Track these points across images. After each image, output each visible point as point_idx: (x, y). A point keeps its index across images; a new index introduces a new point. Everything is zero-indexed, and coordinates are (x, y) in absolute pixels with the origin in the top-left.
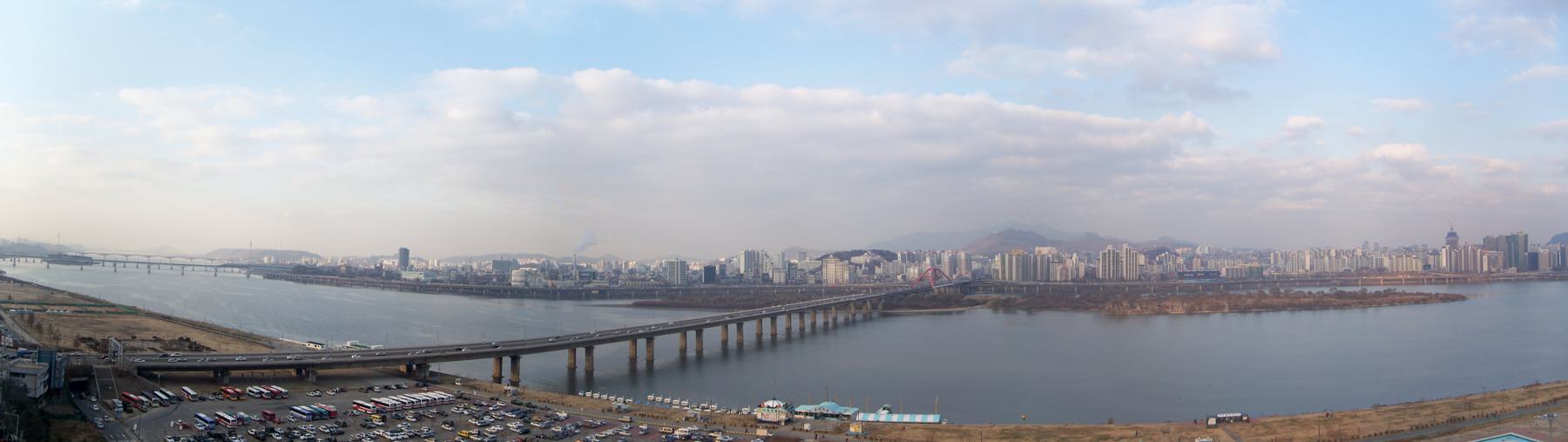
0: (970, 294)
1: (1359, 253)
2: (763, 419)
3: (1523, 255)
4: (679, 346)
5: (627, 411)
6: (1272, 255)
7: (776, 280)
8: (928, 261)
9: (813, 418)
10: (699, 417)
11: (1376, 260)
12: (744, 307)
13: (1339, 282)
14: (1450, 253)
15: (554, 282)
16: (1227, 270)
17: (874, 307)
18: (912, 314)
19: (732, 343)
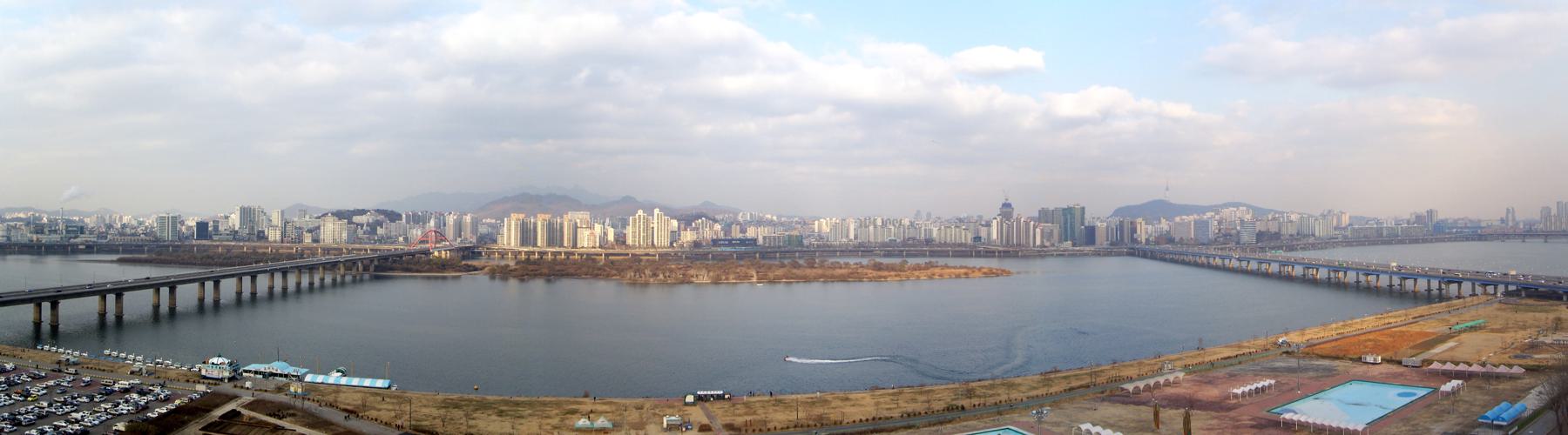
0: (473, 258)
1: (906, 222)
2: (207, 376)
3: (1079, 229)
4: (32, 320)
5: (75, 364)
6: (816, 222)
7: (271, 238)
8: (432, 223)
9: (261, 376)
10: (144, 371)
11: (925, 230)
12: (221, 265)
13: (882, 253)
14: (1002, 225)
15: (39, 236)
16: (764, 238)
17: (366, 269)
18: (405, 277)
19: (209, 299)
